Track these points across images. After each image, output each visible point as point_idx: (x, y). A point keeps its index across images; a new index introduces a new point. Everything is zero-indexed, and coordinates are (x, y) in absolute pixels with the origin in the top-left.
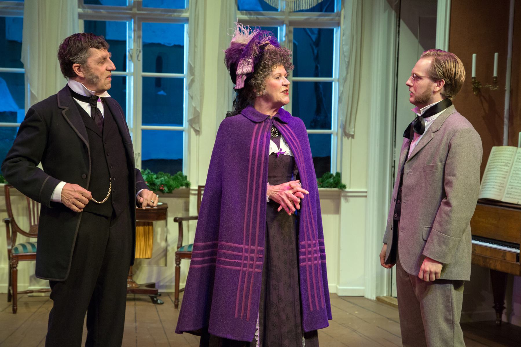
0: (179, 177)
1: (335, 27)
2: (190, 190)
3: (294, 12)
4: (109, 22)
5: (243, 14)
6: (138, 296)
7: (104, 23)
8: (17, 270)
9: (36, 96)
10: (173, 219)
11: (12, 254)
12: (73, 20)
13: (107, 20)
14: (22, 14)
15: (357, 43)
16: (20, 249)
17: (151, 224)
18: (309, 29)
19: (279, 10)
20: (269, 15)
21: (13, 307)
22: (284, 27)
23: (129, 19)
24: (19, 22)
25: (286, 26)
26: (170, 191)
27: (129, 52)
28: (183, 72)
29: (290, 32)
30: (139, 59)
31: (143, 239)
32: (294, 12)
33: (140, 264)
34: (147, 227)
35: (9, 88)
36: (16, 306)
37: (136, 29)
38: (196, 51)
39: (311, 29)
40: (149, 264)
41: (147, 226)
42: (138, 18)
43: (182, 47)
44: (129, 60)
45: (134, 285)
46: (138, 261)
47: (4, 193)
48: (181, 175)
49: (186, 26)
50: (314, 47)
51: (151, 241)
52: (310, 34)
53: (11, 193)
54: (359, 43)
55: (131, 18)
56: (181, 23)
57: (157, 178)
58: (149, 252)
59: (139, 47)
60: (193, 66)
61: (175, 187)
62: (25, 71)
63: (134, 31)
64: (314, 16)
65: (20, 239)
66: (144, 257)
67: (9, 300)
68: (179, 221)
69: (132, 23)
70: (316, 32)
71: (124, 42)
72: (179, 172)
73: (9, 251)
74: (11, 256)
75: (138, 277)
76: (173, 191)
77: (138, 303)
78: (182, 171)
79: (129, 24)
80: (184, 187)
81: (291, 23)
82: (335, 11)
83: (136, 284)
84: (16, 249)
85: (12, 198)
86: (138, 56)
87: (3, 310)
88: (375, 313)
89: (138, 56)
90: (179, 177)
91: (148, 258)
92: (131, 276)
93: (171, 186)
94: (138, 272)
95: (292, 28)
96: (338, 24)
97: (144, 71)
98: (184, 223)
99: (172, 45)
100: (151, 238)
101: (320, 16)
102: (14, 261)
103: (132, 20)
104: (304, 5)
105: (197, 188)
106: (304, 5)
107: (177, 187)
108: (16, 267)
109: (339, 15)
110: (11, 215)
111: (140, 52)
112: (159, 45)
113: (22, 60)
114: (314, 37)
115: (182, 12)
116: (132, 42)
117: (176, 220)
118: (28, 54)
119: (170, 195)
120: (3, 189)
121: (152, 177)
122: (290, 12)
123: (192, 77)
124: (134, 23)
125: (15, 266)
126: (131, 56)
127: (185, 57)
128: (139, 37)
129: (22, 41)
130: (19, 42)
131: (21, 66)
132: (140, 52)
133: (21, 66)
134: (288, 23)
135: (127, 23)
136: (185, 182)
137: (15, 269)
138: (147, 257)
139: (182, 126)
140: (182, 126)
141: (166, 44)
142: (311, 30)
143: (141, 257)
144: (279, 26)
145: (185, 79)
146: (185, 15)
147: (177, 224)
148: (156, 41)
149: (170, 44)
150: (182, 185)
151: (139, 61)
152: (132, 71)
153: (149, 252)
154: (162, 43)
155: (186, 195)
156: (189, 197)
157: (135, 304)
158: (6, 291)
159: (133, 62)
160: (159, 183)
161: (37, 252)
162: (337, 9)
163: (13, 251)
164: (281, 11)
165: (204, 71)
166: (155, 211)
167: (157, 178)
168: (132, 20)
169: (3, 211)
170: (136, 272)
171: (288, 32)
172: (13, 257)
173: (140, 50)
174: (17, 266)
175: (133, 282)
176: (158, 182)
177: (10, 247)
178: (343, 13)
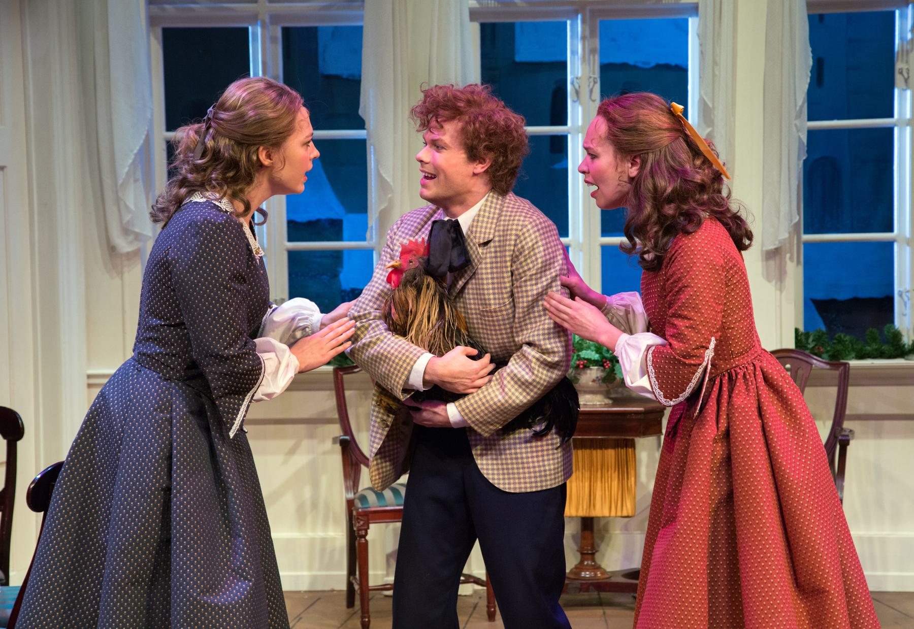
4: (522, 24)
6: (605, 595)
7: (511, 27)
8: (367, 541)
9: (391, 184)
11: (357, 509)
12: (462, 25)
13: (517, 20)
14: (361, 18)
16: (372, 498)
17: (632, 445)
21: (363, 617)
23: (573, 15)
24: (353, 38)
25: (263, 27)
27: (572, 83)
30: (593, 98)
31: (615, 475)
33: (606, 529)
34: (623, 451)
35: (326, 172)
36: (369, 618)
37: (587, 33)
38: (717, 72)
40: (626, 528)
41: (622, 448)
42: (592, 12)
44: (574, 101)
45: (599, 574)
46: (602, 523)
47: (333, 386)
49: (693, 24)
51: (633, 479)
53: (346, 385)
55: (576, 13)
58: (629, 504)
59: (594, 73)
60: (710, 105)
62: (368, 134)
63: (583, 38)
65: (366, 478)
66: (619, 514)
67: (350, 603)
69: (579, 22)
71: (564, 65)
73: (350, 503)
74: (354, 513)
75: (603, 555)
77: (609, 611)
79: (572, 25)
81: (275, 19)
83: (604, 572)
84: (363, 498)
85: (348, 393)
86: (591, 91)
87: (342, 625)
89: (591, 91)
91: (628, 517)
92: (593, 554)
94: (603, 546)
99: (653, 64)
100: (632, 473)
102: (362, 523)
103: (580, 16)
108: (364, 536)
110: (347, 429)
111: (595, 83)
113: (361, 112)
116: (579, 63)
118: (371, 103)
120: (332, 376)
123: (709, 130)
124: (583, 22)
125: (363, 533)
126: (577, 93)
128: (593, 51)
129: (360, 76)
130: (345, 73)
131: (360, 124)
132: (595, 83)
133: (360, 124)
135: (569, 22)
137: (363, 540)
138: (625, 514)
141: (640, 65)
143: (606, 513)
144: (898, 8)
149: (648, 64)
151: (594, 101)
152: (580, 123)
153: (629, 504)
154: (631, 62)
157: (604, 613)
158: (342, 586)
159: (580, 103)
161: (405, 505)
163: (358, 504)
165: (734, 115)
166: (642, 417)
169: (330, 421)
170: (599, 546)
172: (359, 514)
173: (595, 78)
174: (366, 534)
175: (597, 568)
177: (351, 496)
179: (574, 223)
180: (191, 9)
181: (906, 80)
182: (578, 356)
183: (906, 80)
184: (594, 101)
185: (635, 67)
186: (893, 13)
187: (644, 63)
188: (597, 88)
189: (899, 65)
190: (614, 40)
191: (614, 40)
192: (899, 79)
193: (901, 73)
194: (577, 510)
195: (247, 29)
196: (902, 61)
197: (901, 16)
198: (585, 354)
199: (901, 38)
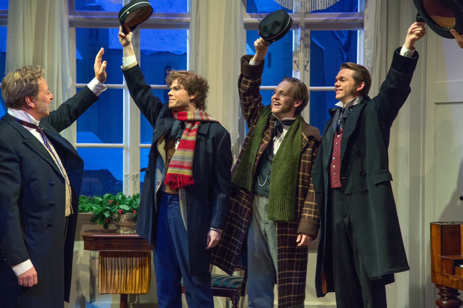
1: (358, 28)
3: (312, 12)
5: (252, 17)
15: (382, 47)
18: (336, 31)
19: (294, 12)
20: (97, 16)
22: (299, 31)
25: (302, 29)
29: (306, 35)
32: (312, 12)
39: (340, 31)
43: (185, 54)
50: (344, 52)
52: (339, 37)
54: (384, 46)
64: (333, 16)
66: (139, 292)
70: (346, 35)
81: (308, 25)
82: (359, 11)
95: (308, 31)
96: (361, 25)
97: (77, 82)
101: (341, 16)
104: (320, 5)
106: (320, 5)
109: (362, 14)
111: (308, 62)
112: (168, 53)
114: (343, 41)
115: (184, 16)
122: (307, 13)
134: (303, 25)
139: (122, 143)
140: (122, 143)
141: (176, 53)
142: (339, 32)
145: (124, 91)
146: (187, 19)
148: (164, 49)
149: (180, 52)
151: (307, 71)
162: (360, 8)
164: (295, 12)
171: (303, 36)
178: (366, 12)
179: (126, 133)
180: (94, 19)
181: (298, 66)
182: (119, 207)
183: (298, 66)
184: (307, 71)
185: (173, 54)
186: (357, 31)
187: (178, 52)
188: (309, 65)
189: (294, 59)
190: (162, 39)
191: (162, 39)
192: (294, 65)
193: (295, 62)
194: (132, 292)
195: (108, 29)
196: (296, 56)
197: (295, 33)
198: (122, 207)
199: (295, 45)
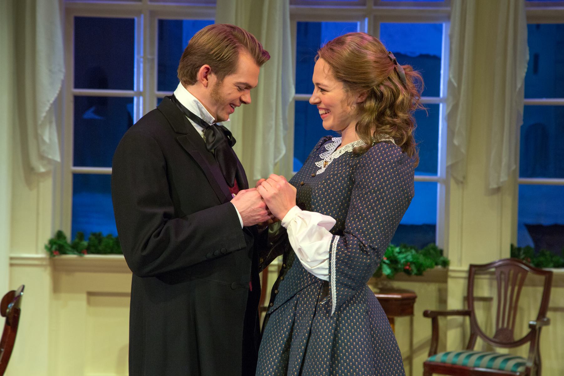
0: (432, 251)
2: (447, 271)
7: (318, 26)
10: (421, 314)
13: (323, 21)
26: (420, 272)
28: (438, 95)
43: (438, 59)
48: (435, 248)
55: (364, 17)
56: (437, 22)
57: (400, 253)
61: (428, 267)
68: (433, 317)
72: (432, 245)
76: (424, 273)
78: (434, 241)
79: (361, 26)
80: (439, 267)
81: (152, 13)
88: (38, 214)
90: (432, 251)
93: (421, 265)
98: (441, 321)
99: (418, 53)
103: (366, 21)
105: (466, 268)
107: (431, 267)
117: (426, 314)
119: (419, 278)
121: (393, 251)
127: (442, 72)
136: (442, 259)
141: (409, 54)
145: (441, 106)
147: (429, 321)
150: (437, 264)
155: (443, 278)
156: (445, 282)
160: (403, 261)
167: (400, 253)
168: (366, 21)
176: (401, 257)
